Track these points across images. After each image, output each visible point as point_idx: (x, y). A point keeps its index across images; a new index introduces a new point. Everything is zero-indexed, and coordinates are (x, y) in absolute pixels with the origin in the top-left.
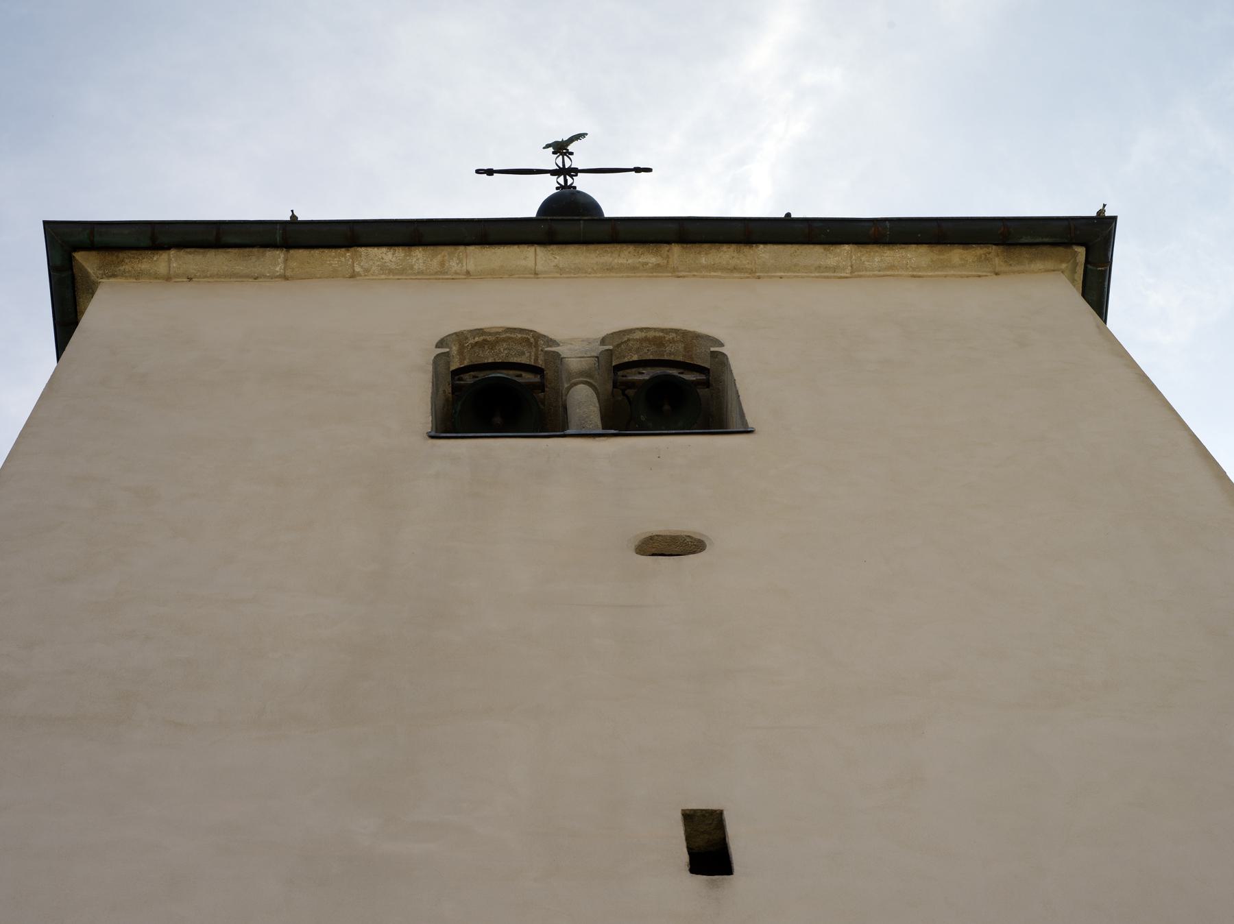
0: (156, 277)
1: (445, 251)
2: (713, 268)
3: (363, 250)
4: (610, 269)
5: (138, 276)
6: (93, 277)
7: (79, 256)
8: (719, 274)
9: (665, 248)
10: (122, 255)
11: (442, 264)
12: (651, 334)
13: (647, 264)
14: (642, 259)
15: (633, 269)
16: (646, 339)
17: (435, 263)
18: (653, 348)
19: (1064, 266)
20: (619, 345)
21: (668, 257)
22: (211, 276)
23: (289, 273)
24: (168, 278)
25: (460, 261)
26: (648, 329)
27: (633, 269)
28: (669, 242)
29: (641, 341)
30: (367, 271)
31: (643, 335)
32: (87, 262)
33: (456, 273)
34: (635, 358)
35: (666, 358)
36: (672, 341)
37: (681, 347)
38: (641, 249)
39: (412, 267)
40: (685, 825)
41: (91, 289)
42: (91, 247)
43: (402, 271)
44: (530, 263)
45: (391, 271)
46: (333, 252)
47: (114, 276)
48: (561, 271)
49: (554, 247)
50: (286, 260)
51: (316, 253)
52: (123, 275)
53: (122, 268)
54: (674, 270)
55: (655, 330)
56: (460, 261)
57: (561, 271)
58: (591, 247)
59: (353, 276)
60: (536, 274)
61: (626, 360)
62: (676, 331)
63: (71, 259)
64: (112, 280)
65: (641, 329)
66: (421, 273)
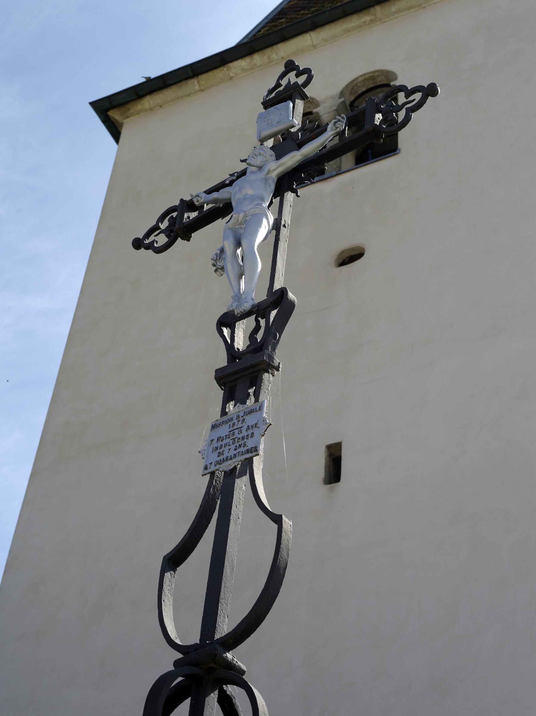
0: (146, 110)
1: (268, 51)
2: (399, 11)
3: (230, 65)
4: (348, 31)
5: (138, 113)
6: (120, 121)
7: (111, 113)
8: (403, 13)
9: (372, 10)
10: (128, 106)
11: (269, 58)
12: (367, 76)
13: (365, 22)
14: (363, 20)
15: (360, 26)
16: (366, 79)
17: (265, 59)
18: (371, 82)
19: (239, 315)
20: (352, 88)
21: (375, 14)
22: (169, 102)
23: (202, 88)
24: (151, 109)
25: (277, 54)
26: (364, 75)
27: (360, 26)
28: (373, 6)
29: (364, 81)
30: (236, 74)
31: (363, 78)
32: (114, 114)
33: (277, 60)
34: (364, 89)
35: (379, 84)
36: (378, 76)
37: (383, 77)
38: (360, 15)
39: (256, 65)
40: (334, 444)
41: (121, 125)
42: (113, 107)
43: (252, 68)
44: (309, 42)
45: (247, 70)
46: (218, 71)
47: (128, 117)
48: (326, 40)
49: (318, 30)
50: (199, 82)
51: (210, 73)
52: (132, 115)
53: (130, 112)
54: (380, 20)
55: (368, 73)
56: (277, 54)
57: (326, 40)
58: (336, 23)
59: (231, 78)
60: (314, 46)
61: (360, 92)
62: (378, 71)
63: (108, 116)
64: (129, 119)
65: (361, 76)
66: (261, 66)
